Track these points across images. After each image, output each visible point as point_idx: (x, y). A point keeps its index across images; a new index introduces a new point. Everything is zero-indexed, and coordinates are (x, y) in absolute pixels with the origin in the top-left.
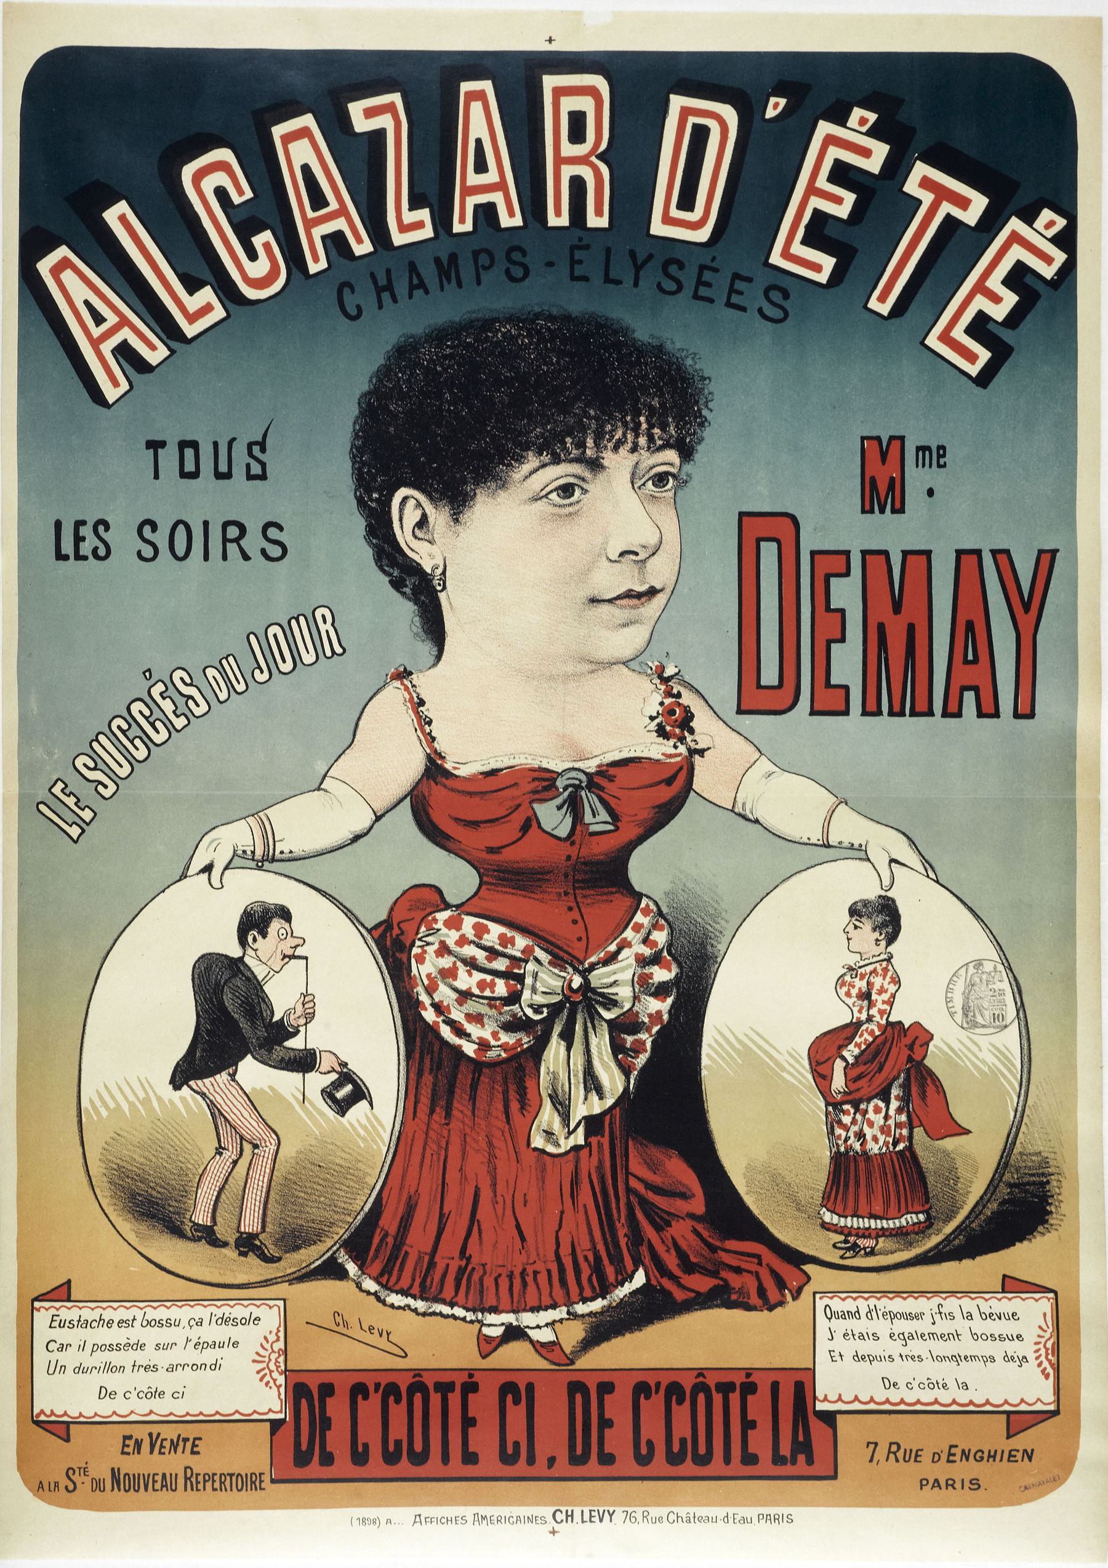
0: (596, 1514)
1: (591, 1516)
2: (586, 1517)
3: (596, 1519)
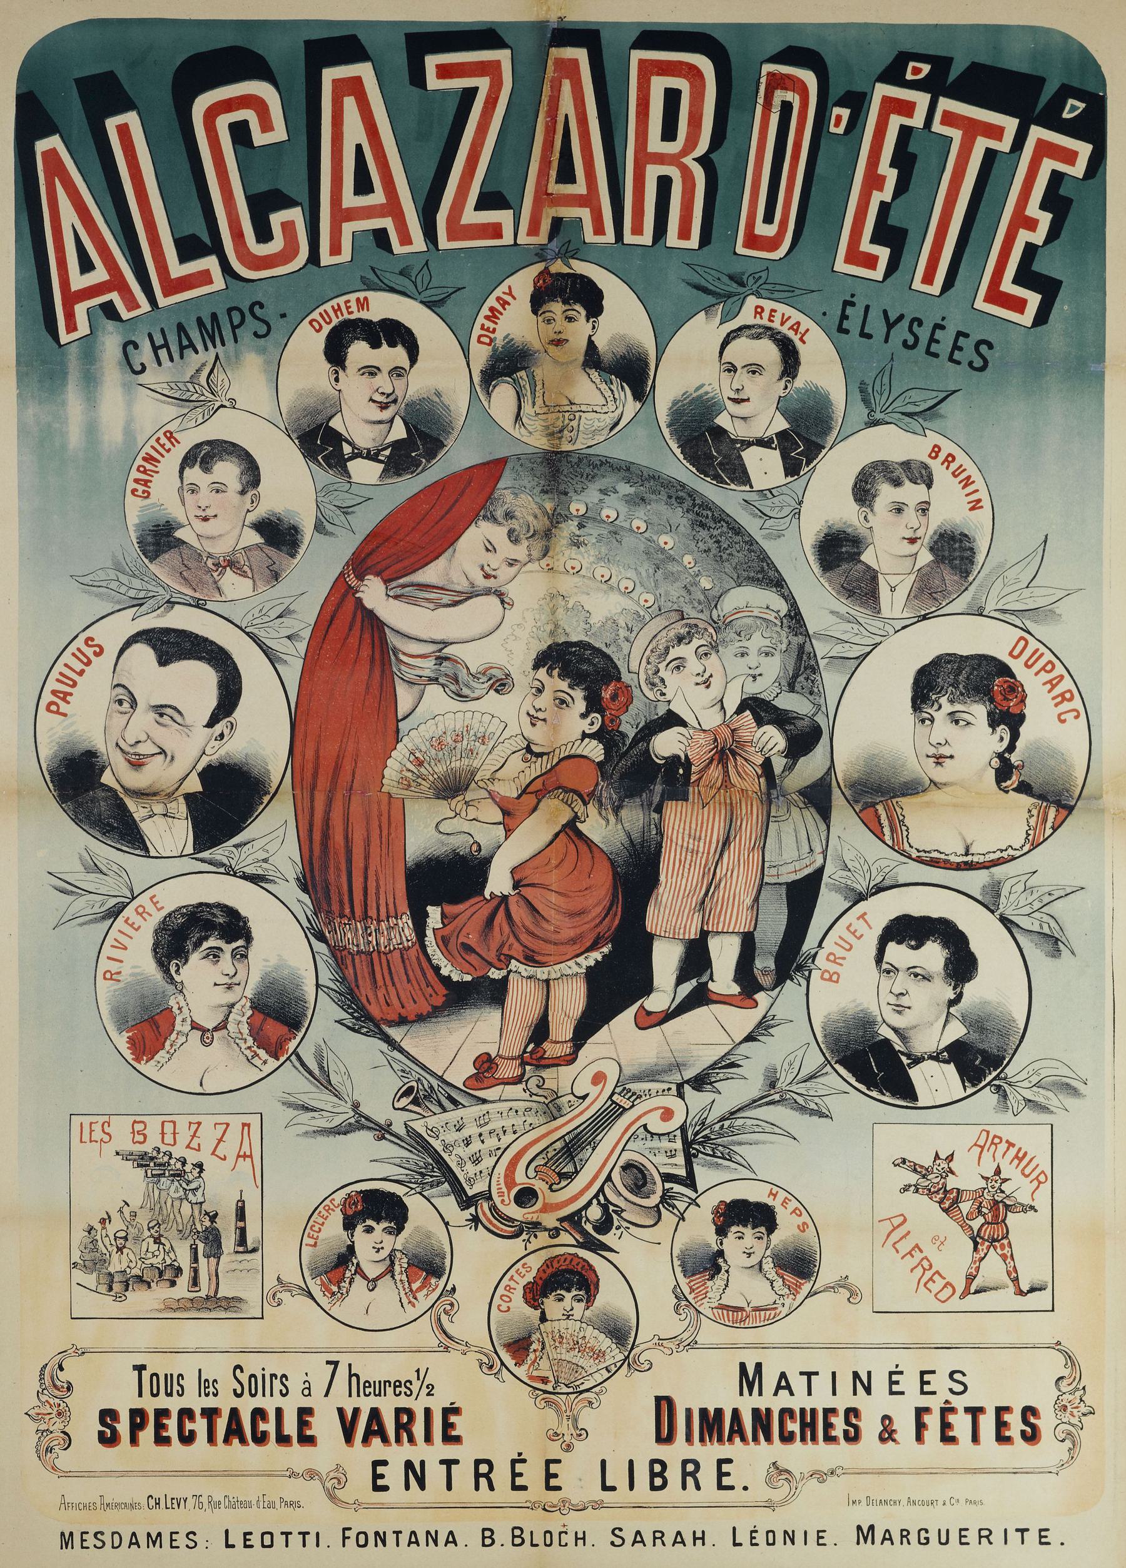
0: (175, 1501)
1: (312, 1237)
2: (169, 1505)
3: (175, 1506)
